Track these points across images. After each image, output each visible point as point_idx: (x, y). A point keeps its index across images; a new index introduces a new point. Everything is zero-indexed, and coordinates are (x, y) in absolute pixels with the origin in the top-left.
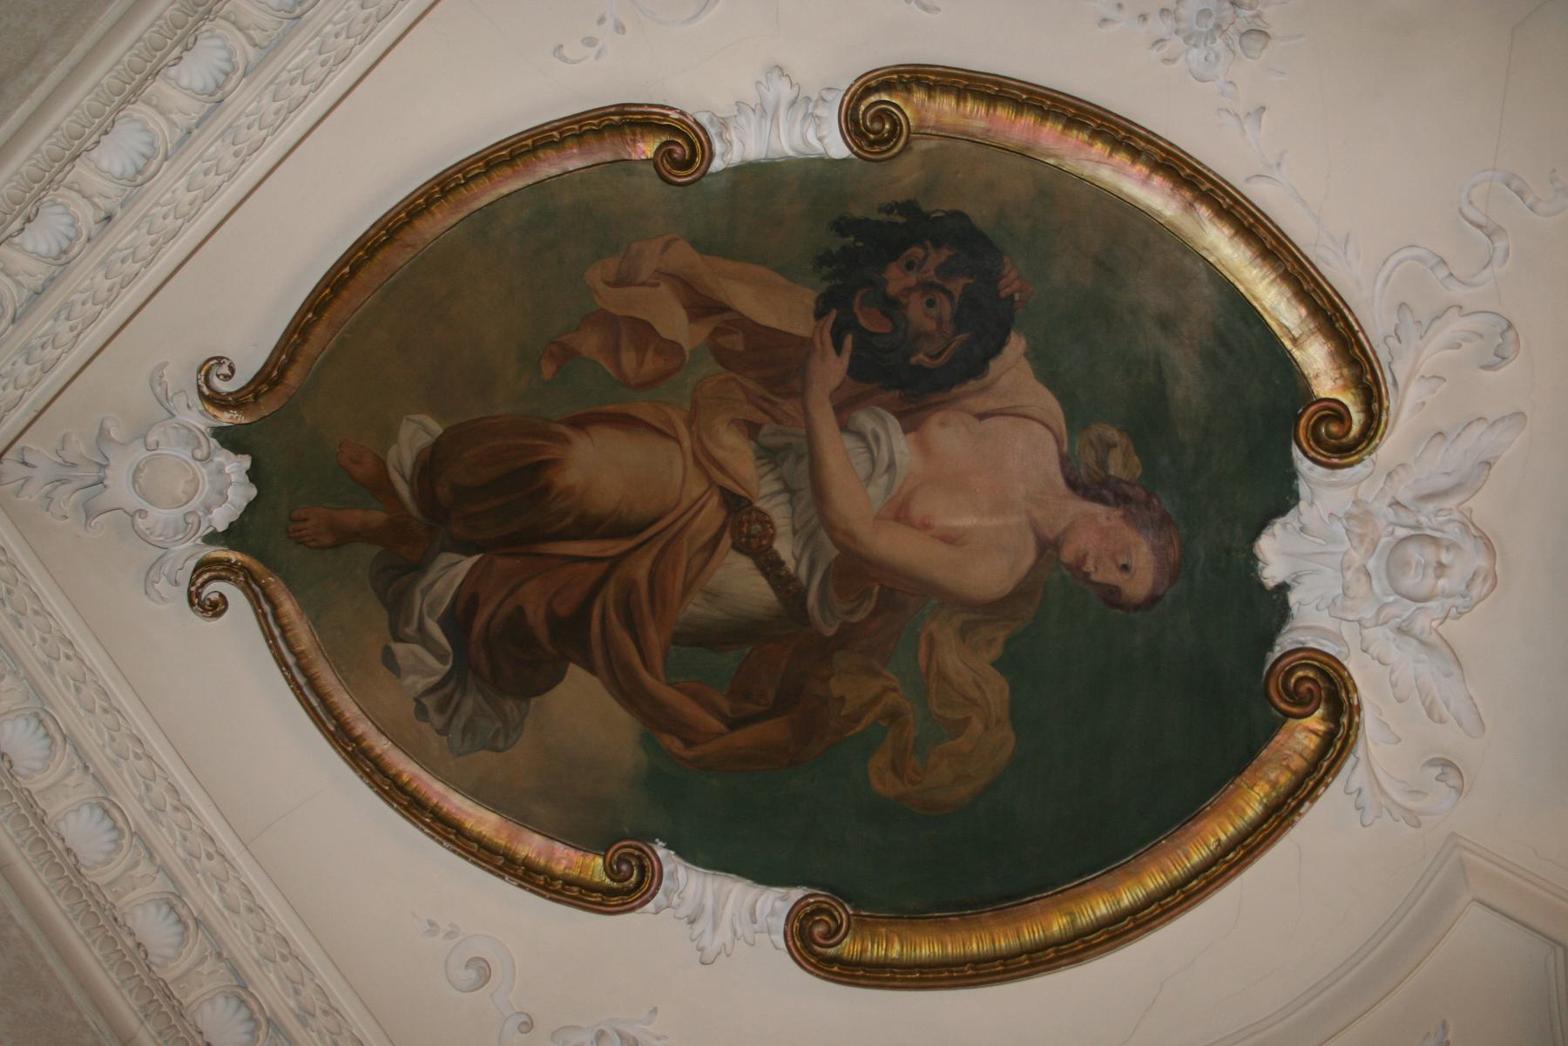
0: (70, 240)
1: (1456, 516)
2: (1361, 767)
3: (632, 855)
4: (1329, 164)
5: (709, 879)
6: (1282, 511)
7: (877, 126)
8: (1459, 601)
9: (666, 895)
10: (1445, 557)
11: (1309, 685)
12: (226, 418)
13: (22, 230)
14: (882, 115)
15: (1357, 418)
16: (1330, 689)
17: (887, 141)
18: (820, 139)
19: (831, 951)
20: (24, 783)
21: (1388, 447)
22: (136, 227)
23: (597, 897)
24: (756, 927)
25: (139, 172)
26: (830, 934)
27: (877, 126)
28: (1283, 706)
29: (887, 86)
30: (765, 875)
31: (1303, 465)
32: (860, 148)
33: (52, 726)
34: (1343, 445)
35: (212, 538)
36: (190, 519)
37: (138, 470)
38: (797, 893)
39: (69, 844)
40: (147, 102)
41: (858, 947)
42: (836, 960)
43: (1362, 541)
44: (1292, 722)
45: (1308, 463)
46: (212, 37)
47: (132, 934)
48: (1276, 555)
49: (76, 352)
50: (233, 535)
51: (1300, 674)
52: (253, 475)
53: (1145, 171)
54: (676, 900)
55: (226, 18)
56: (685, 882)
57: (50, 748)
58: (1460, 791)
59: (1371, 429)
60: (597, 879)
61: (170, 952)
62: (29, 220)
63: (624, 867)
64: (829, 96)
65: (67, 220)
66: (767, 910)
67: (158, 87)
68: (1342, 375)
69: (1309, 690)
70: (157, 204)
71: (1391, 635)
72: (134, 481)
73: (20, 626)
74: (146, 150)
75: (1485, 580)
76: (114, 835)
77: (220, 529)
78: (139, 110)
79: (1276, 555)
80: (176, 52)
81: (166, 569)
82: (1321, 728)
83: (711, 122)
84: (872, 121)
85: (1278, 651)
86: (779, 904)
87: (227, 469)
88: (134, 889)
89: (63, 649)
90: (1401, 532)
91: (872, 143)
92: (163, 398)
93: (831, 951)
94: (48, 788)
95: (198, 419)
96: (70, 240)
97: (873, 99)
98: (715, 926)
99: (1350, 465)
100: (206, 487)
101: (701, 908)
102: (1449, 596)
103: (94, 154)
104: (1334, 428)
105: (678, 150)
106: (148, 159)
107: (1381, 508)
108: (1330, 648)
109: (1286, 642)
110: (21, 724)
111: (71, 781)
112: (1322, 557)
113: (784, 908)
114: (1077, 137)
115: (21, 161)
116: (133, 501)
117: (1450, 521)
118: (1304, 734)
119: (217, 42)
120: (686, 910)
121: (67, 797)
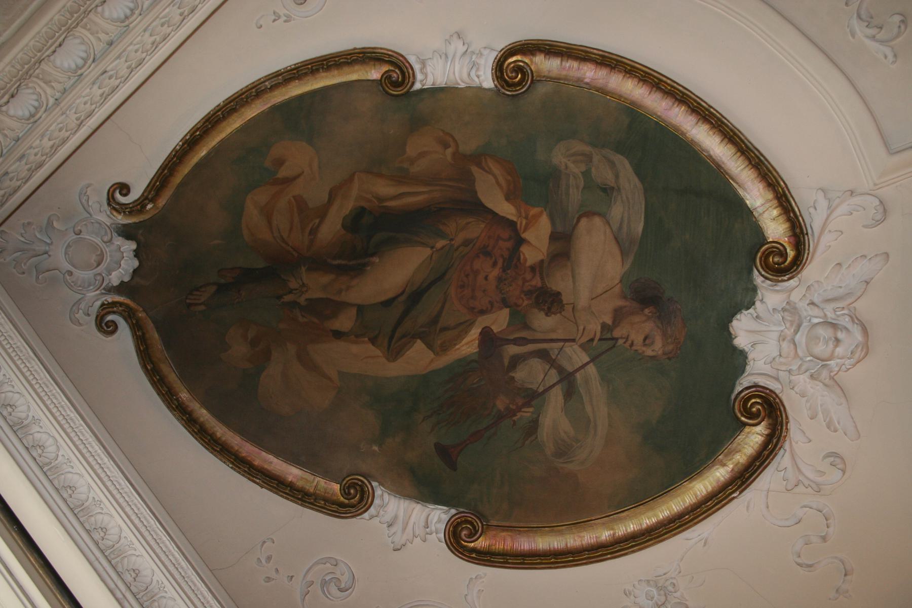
1: (845, 312)
2: (787, 455)
3: (357, 484)
4: (787, 109)
8: (847, 362)
10: (840, 335)
12: (121, 219)
13: (8, 102)
14: (519, 69)
15: (791, 254)
16: (771, 409)
18: (478, 77)
21: (810, 271)
22: (119, 57)
26: (470, 535)
28: (743, 419)
34: (787, 263)
35: (110, 290)
40: (84, 27)
42: (474, 550)
43: (791, 325)
44: (747, 429)
46: (28, 88)
48: (743, 330)
49: (78, 135)
50: (122, 288)
51: (753, 400)
52: (137, 254)
54: (382, 513)
55: (37, 77)
58: (844, 471)
59: (798, 262)
62: (12, 96)
63: (352, 491)
64: (485, 52)
65: (35, 97)
66: (435, 519)
69: (758, 410)
70: (31, 147)
71: (808, 380)
72: (66, 254)
74: (84, 55)
75: (862, 350)
77: (115, 284)
81: (82, 306)
85: (738, 388)
92: (86, 205)
95: (104, 216)
98: (404, 529)
100: (107, 260)
101: (396, 517)
103: (52, 58)
105: (395, 75)
107: (802, 305)
109: (744, 382)
112: (765, 336)
113: (445, 518)
115: (16, 52)
118: (753, 437)
119: (30, 91)
120: (388, 518)
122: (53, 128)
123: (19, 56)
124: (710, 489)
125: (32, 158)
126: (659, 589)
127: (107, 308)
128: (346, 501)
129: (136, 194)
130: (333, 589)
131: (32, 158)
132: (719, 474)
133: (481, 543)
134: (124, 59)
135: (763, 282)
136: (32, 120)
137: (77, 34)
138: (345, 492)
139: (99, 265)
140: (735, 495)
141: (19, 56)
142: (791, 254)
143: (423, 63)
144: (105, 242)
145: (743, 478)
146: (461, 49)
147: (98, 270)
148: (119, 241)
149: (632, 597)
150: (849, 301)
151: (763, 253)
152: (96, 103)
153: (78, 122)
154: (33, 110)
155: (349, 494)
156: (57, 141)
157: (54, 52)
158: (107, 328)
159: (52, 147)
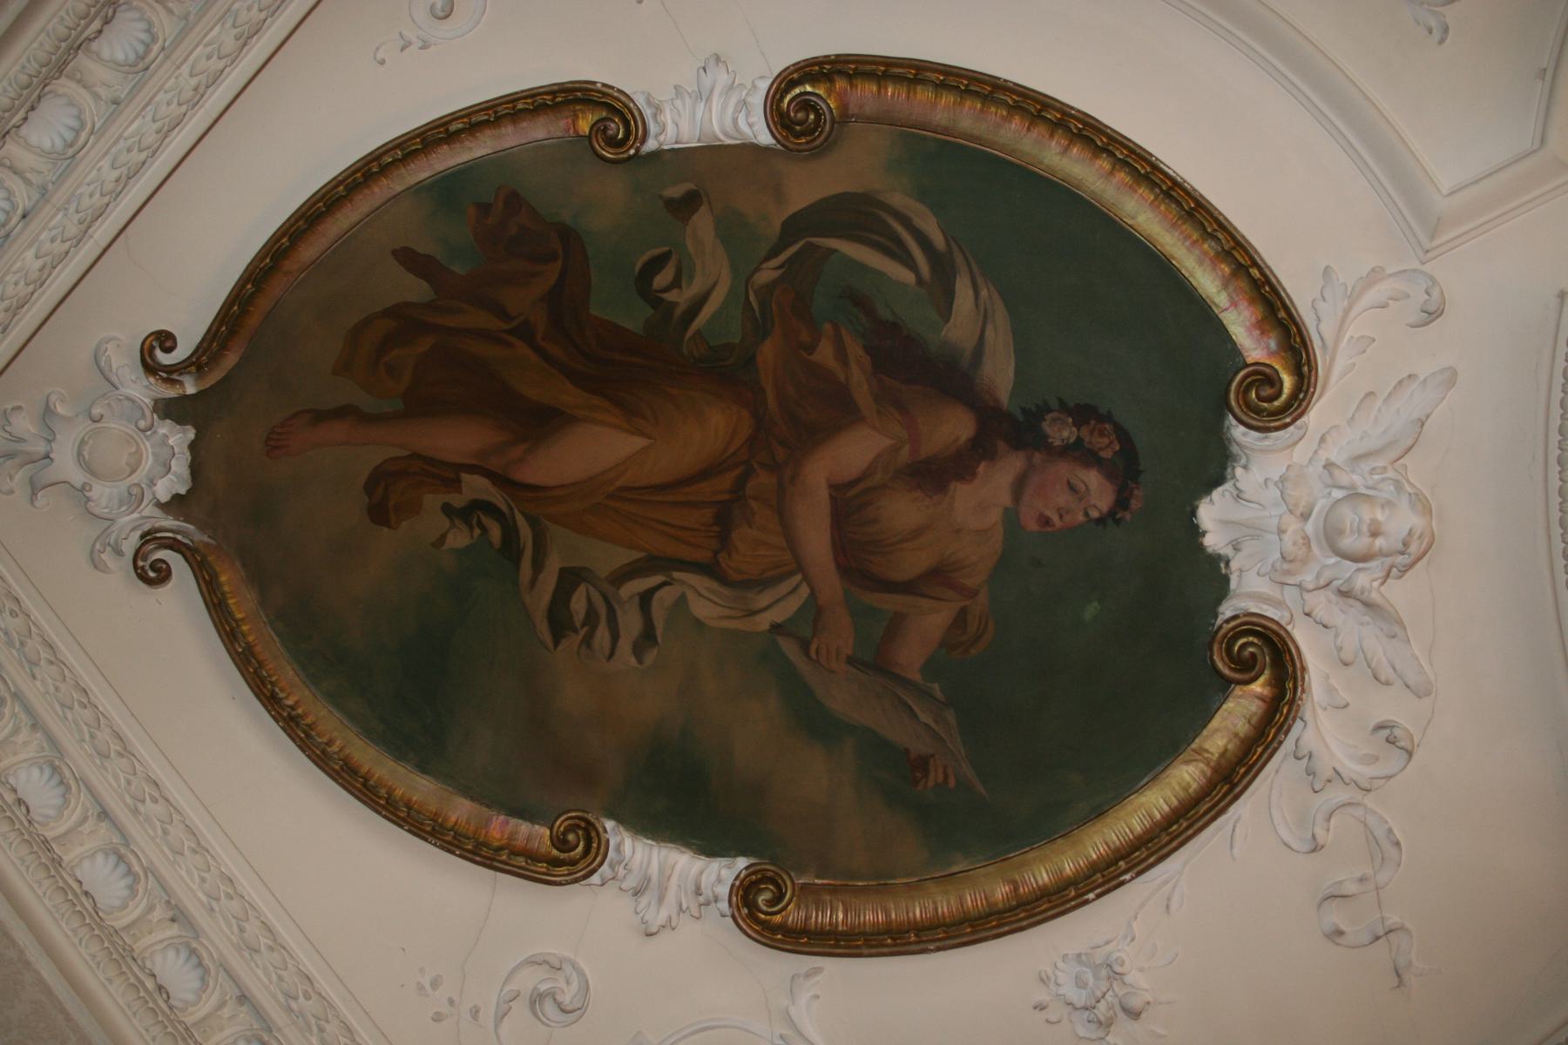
0: (7, 213)
1: (1390, 474)
3: (578, 826)
5: (655, 851)
6: (1219, 481)
7: (800, 115)
8: (1400, 559)
9: (612, 866)
11: (1251, 649)
14: (805, 104)
15: (1288, 382)
16: (1273, 654)
17: (815, 130)
19: (778, 918)
20: (41, 830)
23: (542, 867)
24: (701, 899)
25: (71, 146)
27: (800, 115)
29: (813, 79)
30: (710, 849)
31: (1238, 432)
32: (786, 138)
33: (67, 773)
36: (135, 491)
37: (83, 442)
38: (742, 863)
39: (20, 795)
40: (70, 77)
41: (802, 914)
42: (783, 929)
45: (1242, 428)
47: (15, 791)
50: (176, 505)
53: (1064, 142)
54: (621, 872)
56: (631, 851)
57: (64, 796)
60: (543, 850)
61: (191, 997)
62: (33, 108)
66: (713, 878)
67: (82, 60)
68: (1206, 253)
69: (1252, 654)
71: (1334, 598)
73: (34, 677)
74: (75, 123)
76: (129, 880)
78: (64, 85)
79: (1214, 517)
80: (96, 25)
82: (1266, 691)
83: (656, 136)
84: (796, 112)
86: (724, 872)
87: (171, 442)
88: (221, 1030)
89: (9, 605)
90: (1338, 494)
91: (798, 135)
93: (778, 918)
94: (204, 1019)
95: (142, 390)
96: (7, 213)
97: (797, 91)
98: (661, 899)
99: (1286, 426)
100: (148, 462)
102: (1387, 555)
104: (1267, 391)
106: (78, 132)
108: (1270, 612)
109: (1227, 610)
110: (35, 772)
111: (87, 827)
114: (995, 113)
116: (78, 477)
117: (1383, 480)
118: (1239, 710)
119: (136, 15)
120: (631, 882)
121: (15, 754)
122: (43, 236)
123: (50, 27)
124: (1138, 829)
125: (86, 202)
126: (1096, 968)
127: (150, 537)
128: (562, 856)
129: (181, 353)
130: (549, 1008)
131: (86, 202)
132: (1186, 775)
133: (793, 915)
134: (149, 118)
135: (1244, 434)
136: (141, 66)
137: (61, 91)
138: (560, 842)
139: (133, 472)
140: (1127, 877)
141: (50, 27)
142: (1288, 382)
143: (658, 110)
144: (144, 431)
145: (1230, 780)
146: (723, 78)
147: (135, 478)
148: (165, 428)
149: (1052, 986)
150: (1394, 454)
151: (1237, 393)
152: (111, 192)
153: (83, 227)
154: (69, 136)
155: (565, 841)
156: (48, 259)
157: (25, 119)
158: (154, 576)
159: (41, 269)
